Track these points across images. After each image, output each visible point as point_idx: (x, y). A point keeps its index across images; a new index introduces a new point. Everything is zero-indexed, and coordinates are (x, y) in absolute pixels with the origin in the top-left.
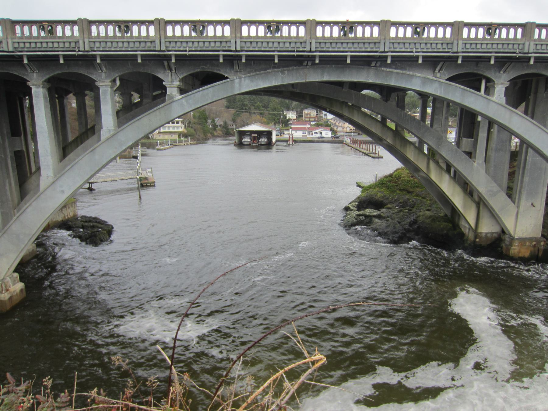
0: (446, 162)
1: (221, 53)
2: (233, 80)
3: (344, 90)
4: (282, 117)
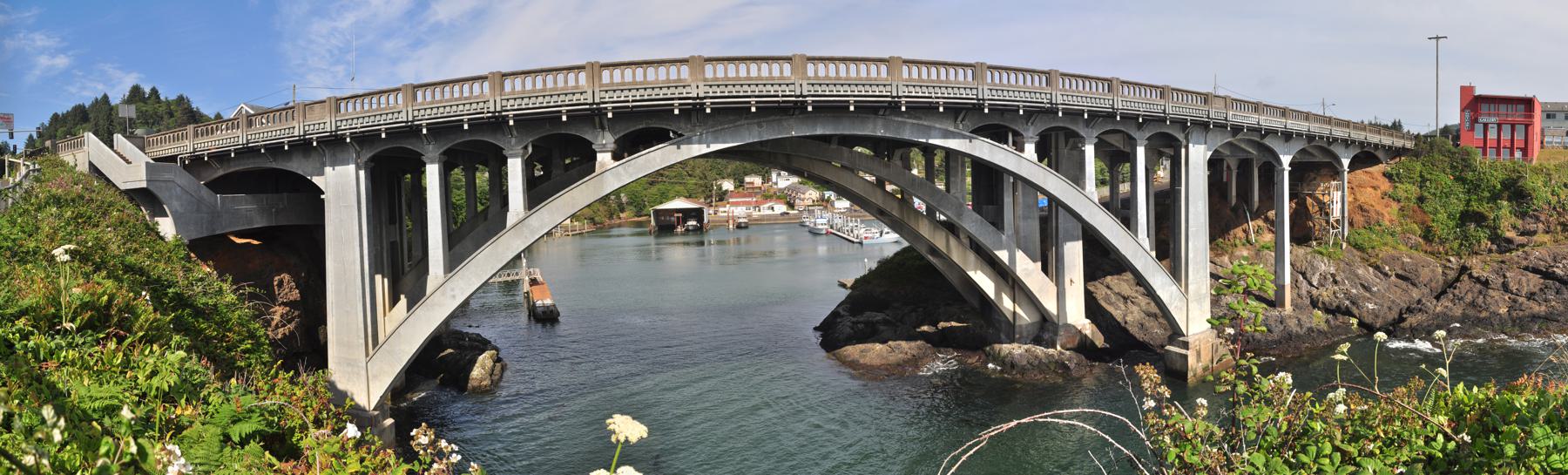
0: (969, 237)
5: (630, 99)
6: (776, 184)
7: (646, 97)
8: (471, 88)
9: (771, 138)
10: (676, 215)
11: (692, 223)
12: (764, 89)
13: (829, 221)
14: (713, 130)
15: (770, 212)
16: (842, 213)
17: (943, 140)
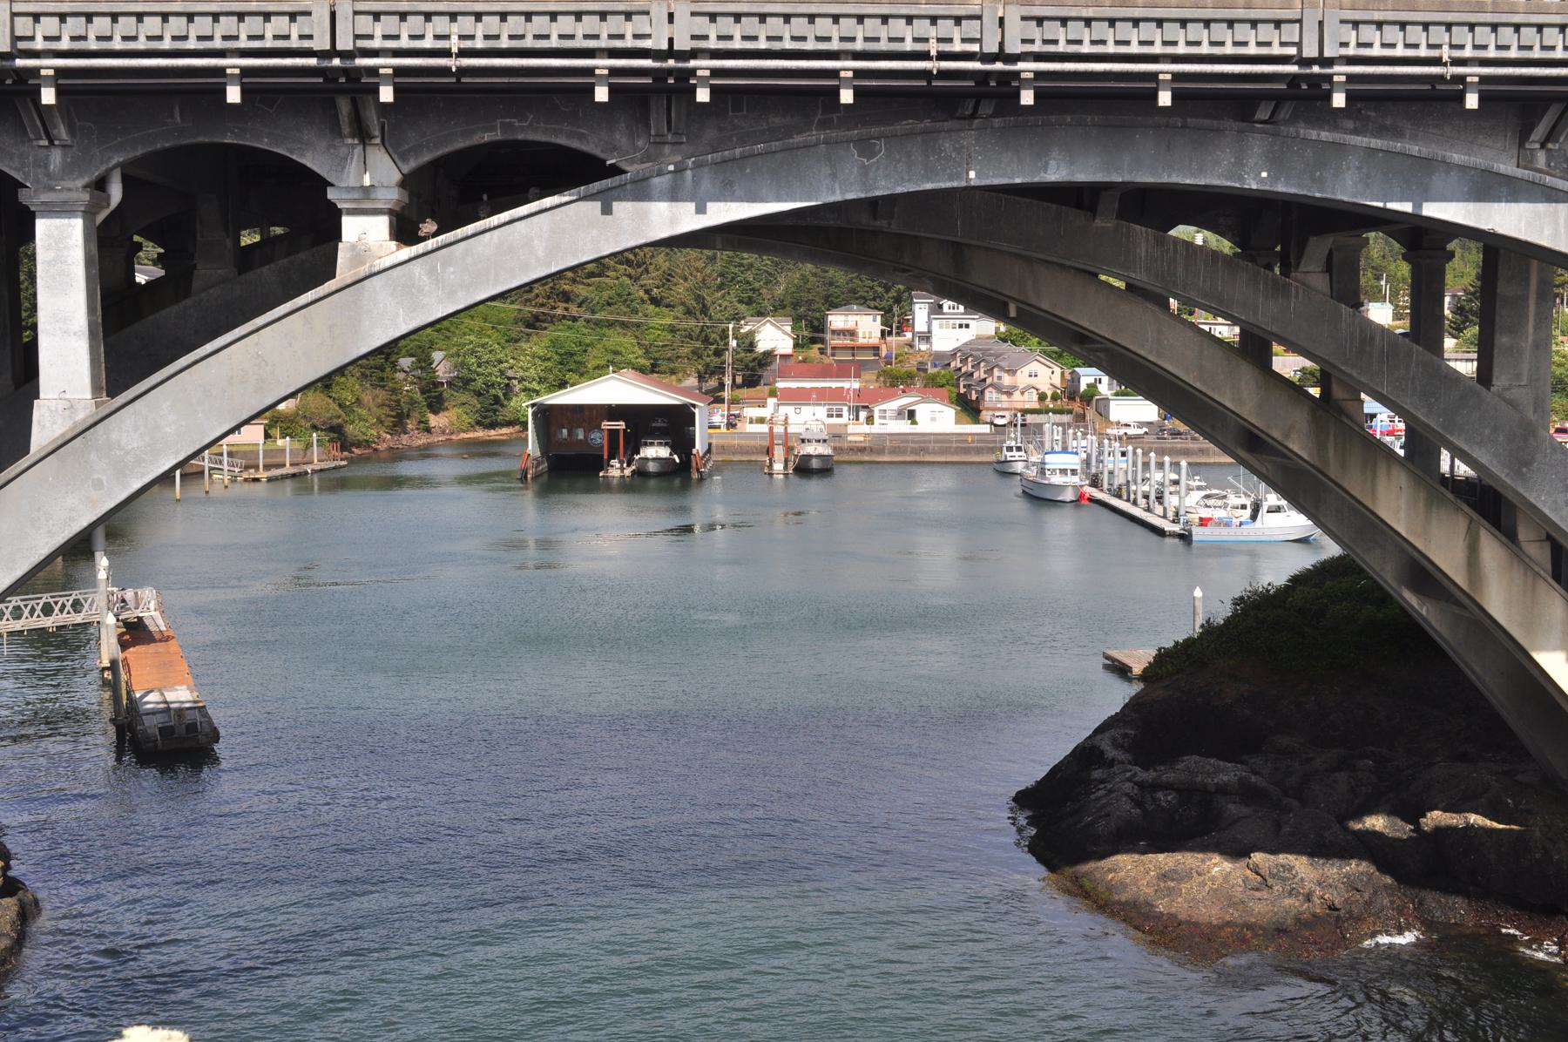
0: (1549, 538)
1: (233, 64)
2: (646, 179)
3: (1098, 222)
4: (733, 343)
6: (926, 337)
7: (505, 43)
9: (899, 190)
10: (607, 425)
11: (656, 452)
13: (1087, 462)
14: (718, 156)
15: (903, 426)
16: (1130, 438)
17: (1471, 206)
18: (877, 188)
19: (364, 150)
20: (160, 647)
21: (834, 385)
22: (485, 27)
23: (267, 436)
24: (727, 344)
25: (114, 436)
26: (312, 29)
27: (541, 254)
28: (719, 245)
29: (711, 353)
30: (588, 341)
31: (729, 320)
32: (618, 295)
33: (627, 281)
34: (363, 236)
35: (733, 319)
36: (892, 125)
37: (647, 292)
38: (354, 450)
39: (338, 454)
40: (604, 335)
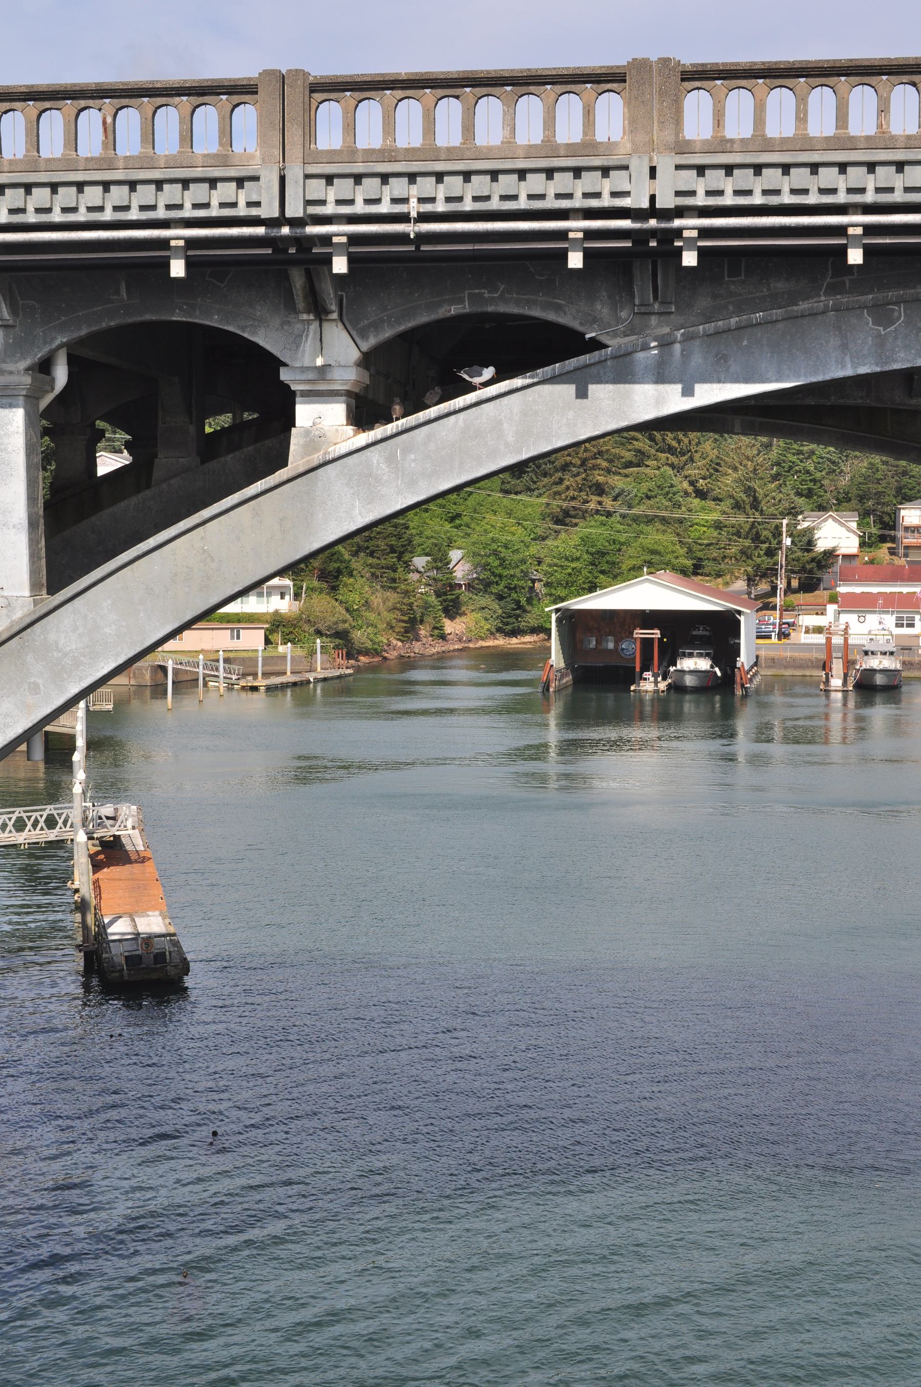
4: (787, 541)
5: (413, 208)
7: (468, 206)
8: (110, 131)
10: (639, 633)
12: (841, 183)
14: (711, 327)
18: (895, 361)
19: (321, 326)
20: (136, 868)
21: (905, 590)
22: (446, 188)
23: (268, 642)
24: (780, 542)
25: (52, 637)
26: (260, 195)
27: (510, 439)
28: (738, 428)
29: (762, 553)
30: (623, 540)
31: (783, 515)
32: (659, 487)
33: (670, 471)
34: (318, 421)
35: (788, 514)
36: (915, 288)
37: (692, 483)
38: (362, 658)
39: (344, 662)
40: (642, 532)
